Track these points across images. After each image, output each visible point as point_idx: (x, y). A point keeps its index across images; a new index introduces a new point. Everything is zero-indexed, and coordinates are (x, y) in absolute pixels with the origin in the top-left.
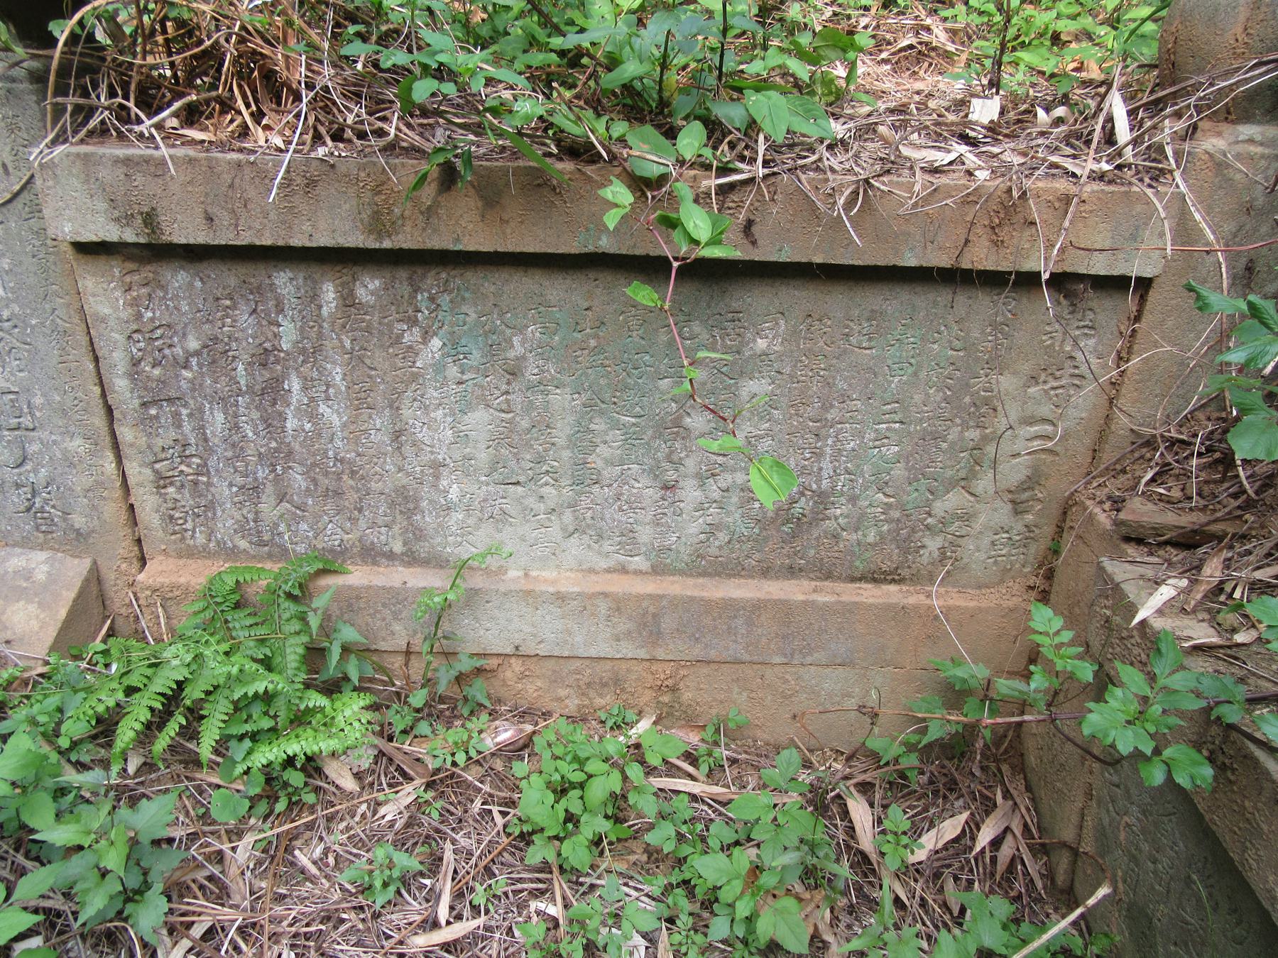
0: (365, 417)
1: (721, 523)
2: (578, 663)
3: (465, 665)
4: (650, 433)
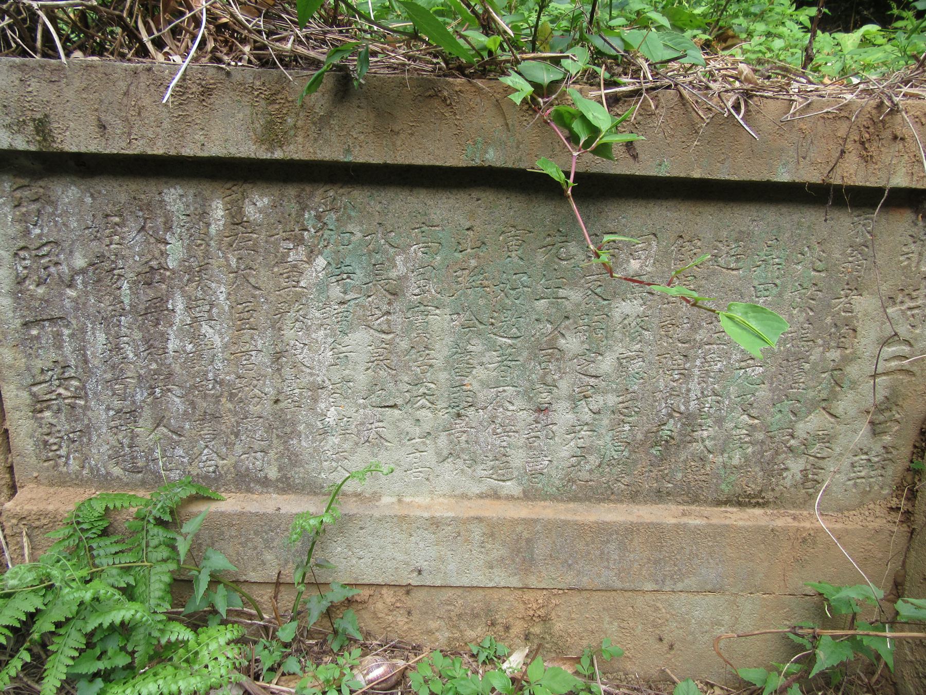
0: (247, 338)
1: (591, 447)
2: (450, 593)
3: (337, 595)
4: (525, 354)
